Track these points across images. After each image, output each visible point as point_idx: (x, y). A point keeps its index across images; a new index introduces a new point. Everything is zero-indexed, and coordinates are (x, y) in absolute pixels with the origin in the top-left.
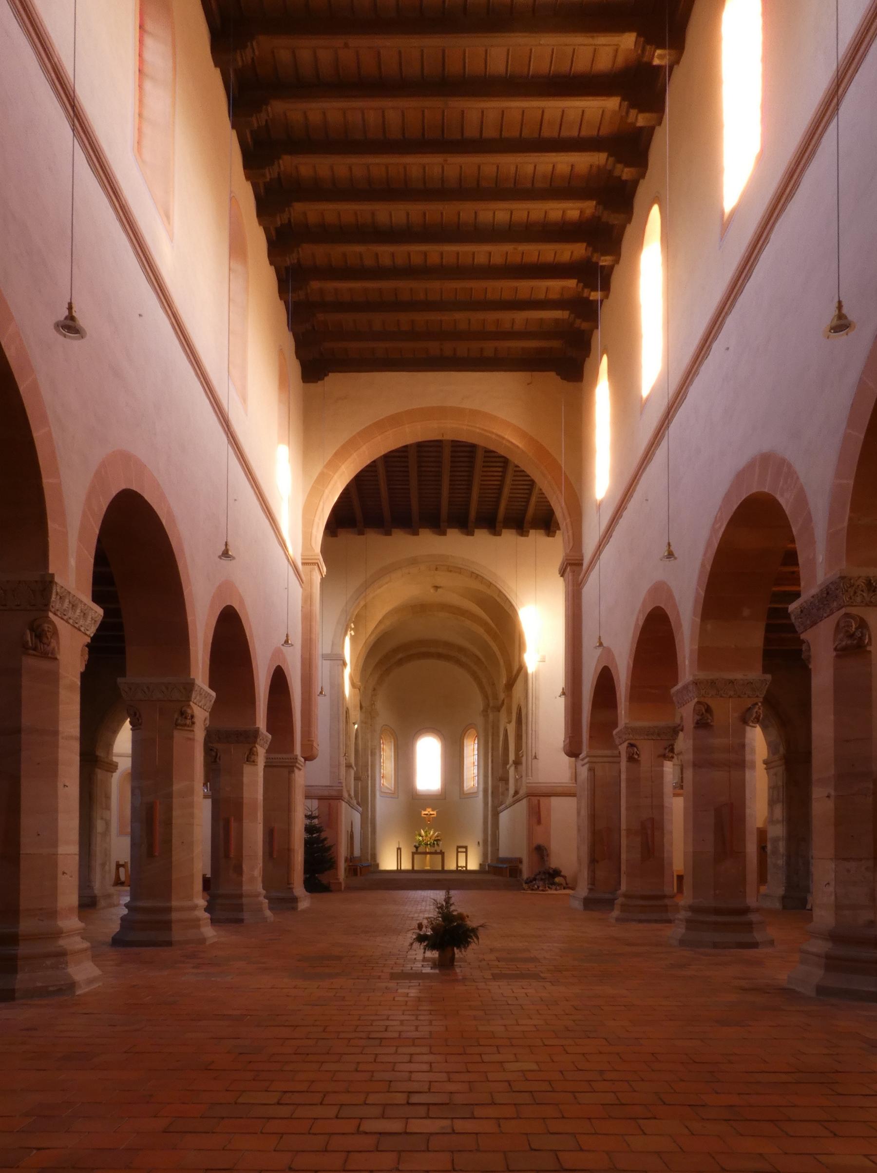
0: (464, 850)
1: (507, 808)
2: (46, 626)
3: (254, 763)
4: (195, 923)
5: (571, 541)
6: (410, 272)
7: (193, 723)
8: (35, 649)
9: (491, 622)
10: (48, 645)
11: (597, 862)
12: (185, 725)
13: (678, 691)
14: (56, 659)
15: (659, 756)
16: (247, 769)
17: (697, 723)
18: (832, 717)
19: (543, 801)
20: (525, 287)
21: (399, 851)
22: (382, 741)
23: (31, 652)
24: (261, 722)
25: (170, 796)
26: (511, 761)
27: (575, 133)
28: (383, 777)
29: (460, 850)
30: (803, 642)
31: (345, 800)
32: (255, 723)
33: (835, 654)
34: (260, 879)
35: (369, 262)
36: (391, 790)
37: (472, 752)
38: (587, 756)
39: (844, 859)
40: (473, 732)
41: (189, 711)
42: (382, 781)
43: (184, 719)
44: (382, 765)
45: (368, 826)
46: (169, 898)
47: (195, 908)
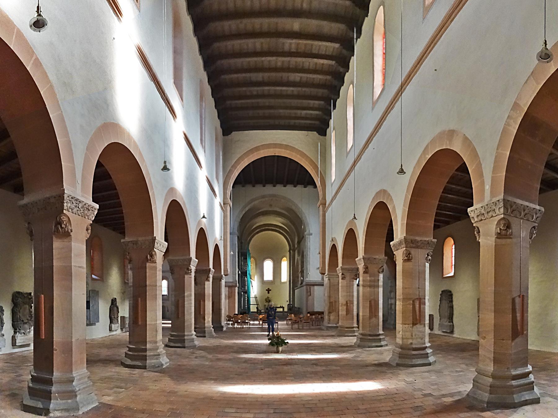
1: (298, 288)
2: (153, 253)
3: (209, 281)
4: (192, 340)
5: (322, 195)
6: (263, 96)
7: (191, 272)
8: (150, 260)
10: (154, 258)
11: (331, 313)
12: (189, 273)
13: (358, 260)
14: (156, 262)
15: (353, 278)
16: (206, 283)
17: (364, 272)
18: (402, 280)
19: (312, 287)
20: (306, 102)
23: (149, 261)
24: (211, 266)
25: (184, 297)
26: (300, 271)
27: (323, 53)
30: (394, 254)
32: (209, 267)
33: (402, 261)
34: (211, 322)
35: (248, 93)
37: (285, 265)
38: (328, 275)
39: (405, 324)
40: (285, 258)
41: (190, 268)
43: (188, 271)
46: (184, 332)
47: (192, 335)
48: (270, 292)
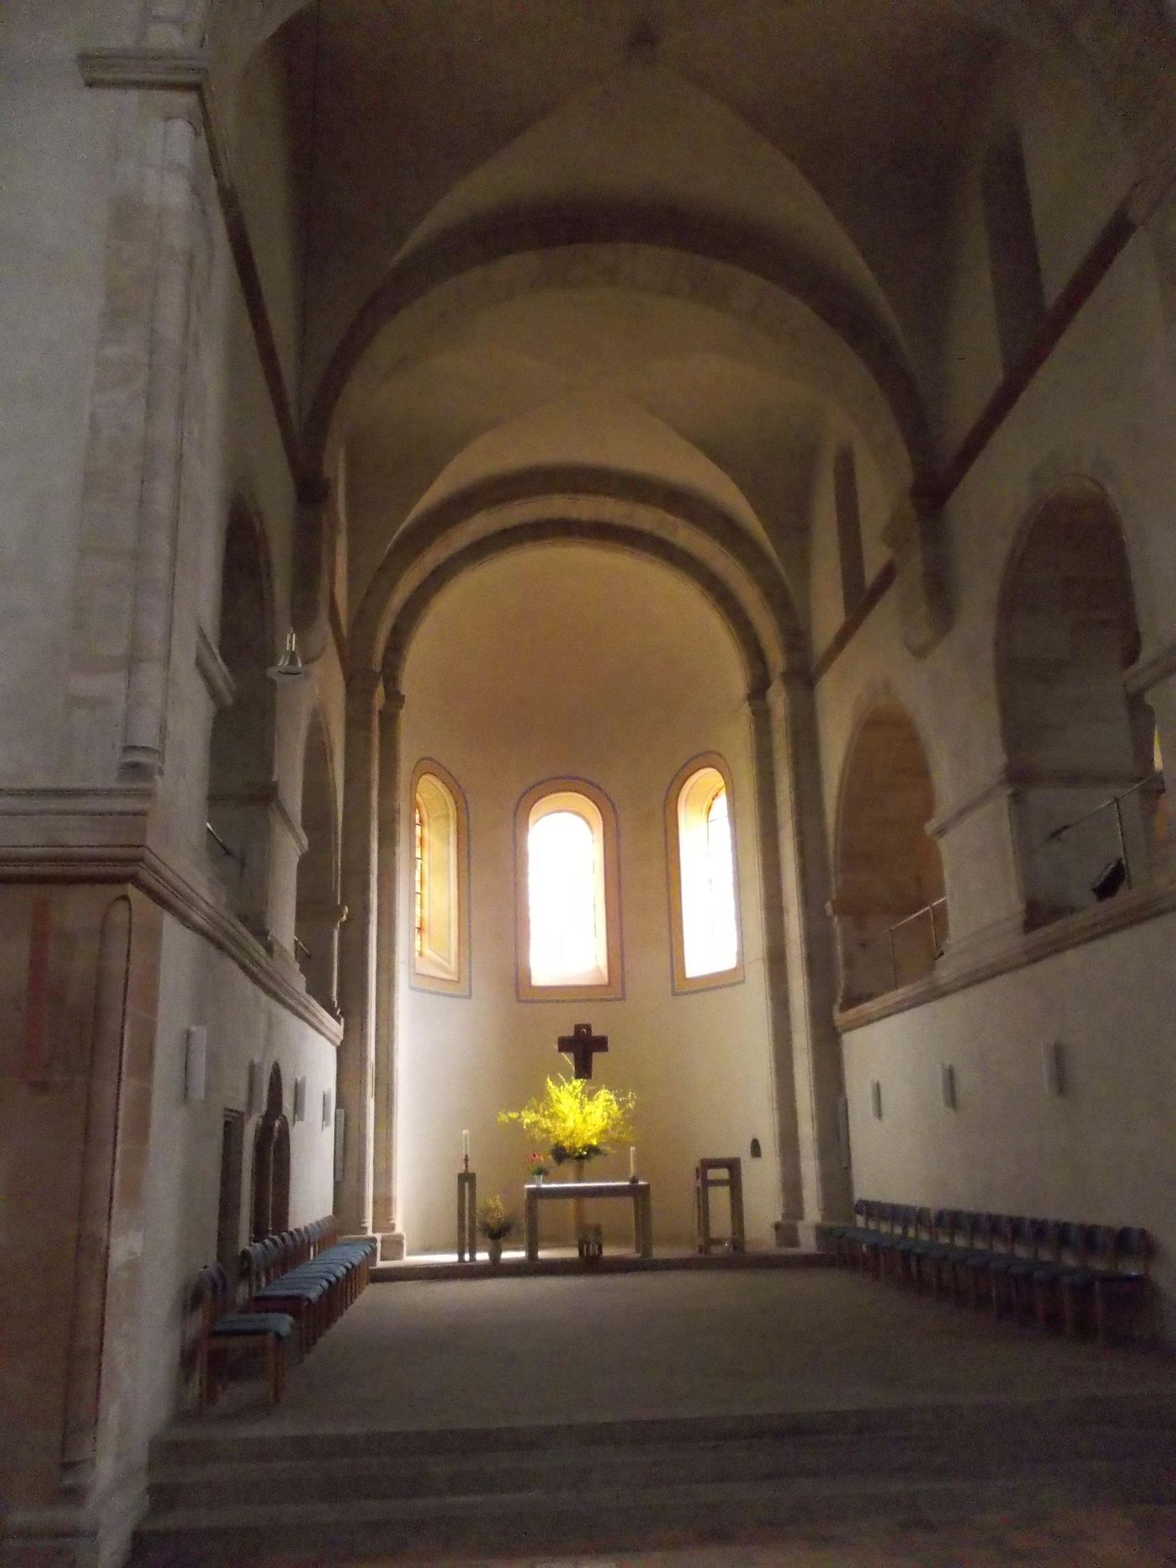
0: (724, 1174)
9: (867, 274)
21: (467, 1185)
22: (417, 816)
28: (420, 929)
29: (713, 1174)
31: (197, 918)
36: (447, 972)
42: (418, 943)
44: (418, 889)
45: (938, 904)
48: (597, 1058)
